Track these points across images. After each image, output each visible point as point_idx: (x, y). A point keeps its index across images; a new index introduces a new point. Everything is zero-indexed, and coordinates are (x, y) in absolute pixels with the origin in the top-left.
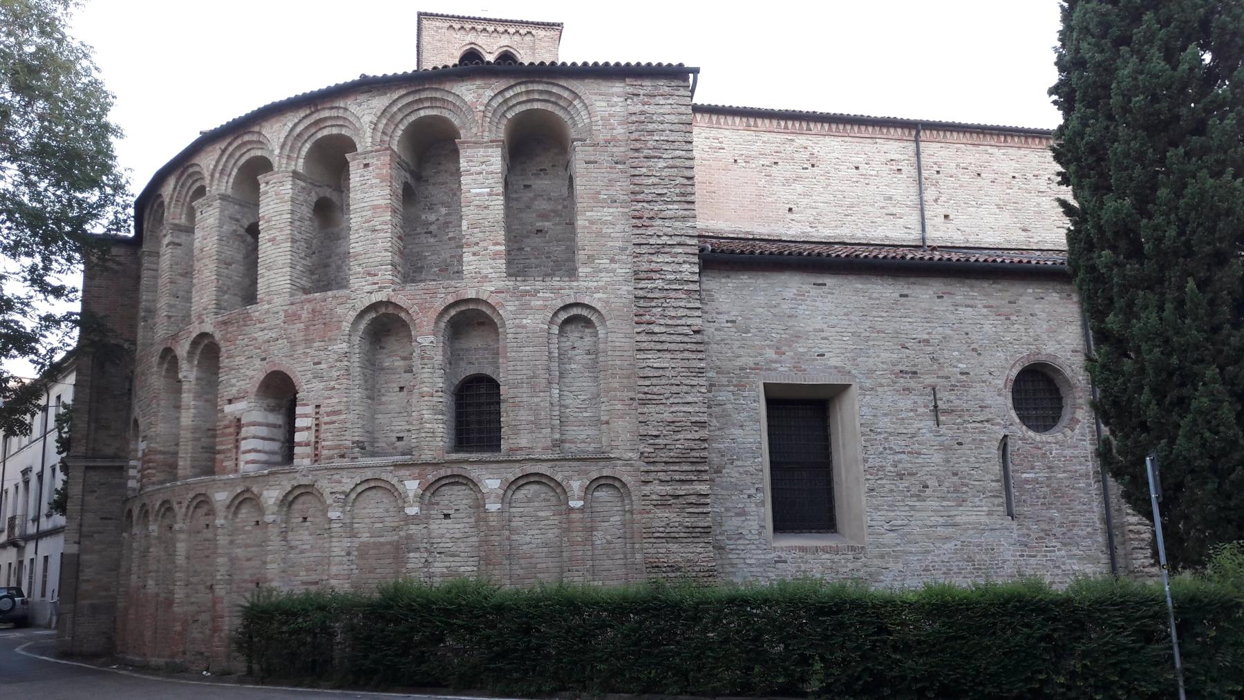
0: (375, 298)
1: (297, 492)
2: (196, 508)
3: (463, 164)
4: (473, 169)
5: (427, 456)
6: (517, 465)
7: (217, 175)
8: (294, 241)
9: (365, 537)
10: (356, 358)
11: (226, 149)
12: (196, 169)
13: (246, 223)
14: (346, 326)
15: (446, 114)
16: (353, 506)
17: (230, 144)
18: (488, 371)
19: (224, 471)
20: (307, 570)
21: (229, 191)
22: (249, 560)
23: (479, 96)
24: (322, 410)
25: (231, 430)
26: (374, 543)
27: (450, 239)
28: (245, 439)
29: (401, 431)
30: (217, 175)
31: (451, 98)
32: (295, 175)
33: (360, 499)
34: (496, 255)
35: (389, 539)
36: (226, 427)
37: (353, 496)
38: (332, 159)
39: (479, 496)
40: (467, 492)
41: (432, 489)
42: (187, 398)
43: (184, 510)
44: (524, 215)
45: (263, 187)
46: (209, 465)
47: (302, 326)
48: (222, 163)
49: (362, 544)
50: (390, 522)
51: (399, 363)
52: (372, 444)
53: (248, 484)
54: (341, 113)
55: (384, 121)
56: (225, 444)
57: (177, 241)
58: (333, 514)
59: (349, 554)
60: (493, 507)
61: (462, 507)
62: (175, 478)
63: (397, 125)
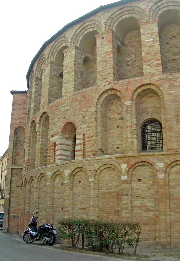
0: (106, 88)
1: (76, 171)
2: (41, 179)
3: (142, 31)
4: (146, 33)
5: (130, 153)
6: (171, 156)
7: (50, 56)
8: (75, 72)
9: (104, 190)
10: (99, 114)
11: (53, 46)
12: (44, 56)
13: (60, 72)
14: (95, 101)
15: (134, 15)
16: (99, 176)
17: (54, 44)
18: (155, 116)
19: (50, 163)
20: (81, 203)
21: (54, 60)
22: (59, 199)
23: (147, 5)
24: (86, 136)
25: (53, 147)
26: (108, 192)
27: (136, 66)
28: (57, 150)
29: (118, 145)
30: (50, 56)
31: (136, 9)
32: (76, 48)
33: (102, 173)
34: (157, 66)
35: (114, 190)
36: (51, 146)
37: (99, 172)
38: (90, 41)
39: (154, 171)
40: (149, 169)
41: (132, 167)
42: (39, 138)
43: (37, 180)
44: (167, 54)
45: (65, 55)
46: (45, 161)
47: (78, 103)
48: (52, 51)
49: (103, 192)
50: (115, 183)
51: (117, 116)
52: (106, 150)
53: (58, 168)
54: (93, 22)
55: (110, 22)
56: (50, 153)
57: (37, 83)
58: (91, 180)
59: (98, 196)
60: (161, 176)
61: (146, 176)
62: (34, 168)
63: (114, 23)
